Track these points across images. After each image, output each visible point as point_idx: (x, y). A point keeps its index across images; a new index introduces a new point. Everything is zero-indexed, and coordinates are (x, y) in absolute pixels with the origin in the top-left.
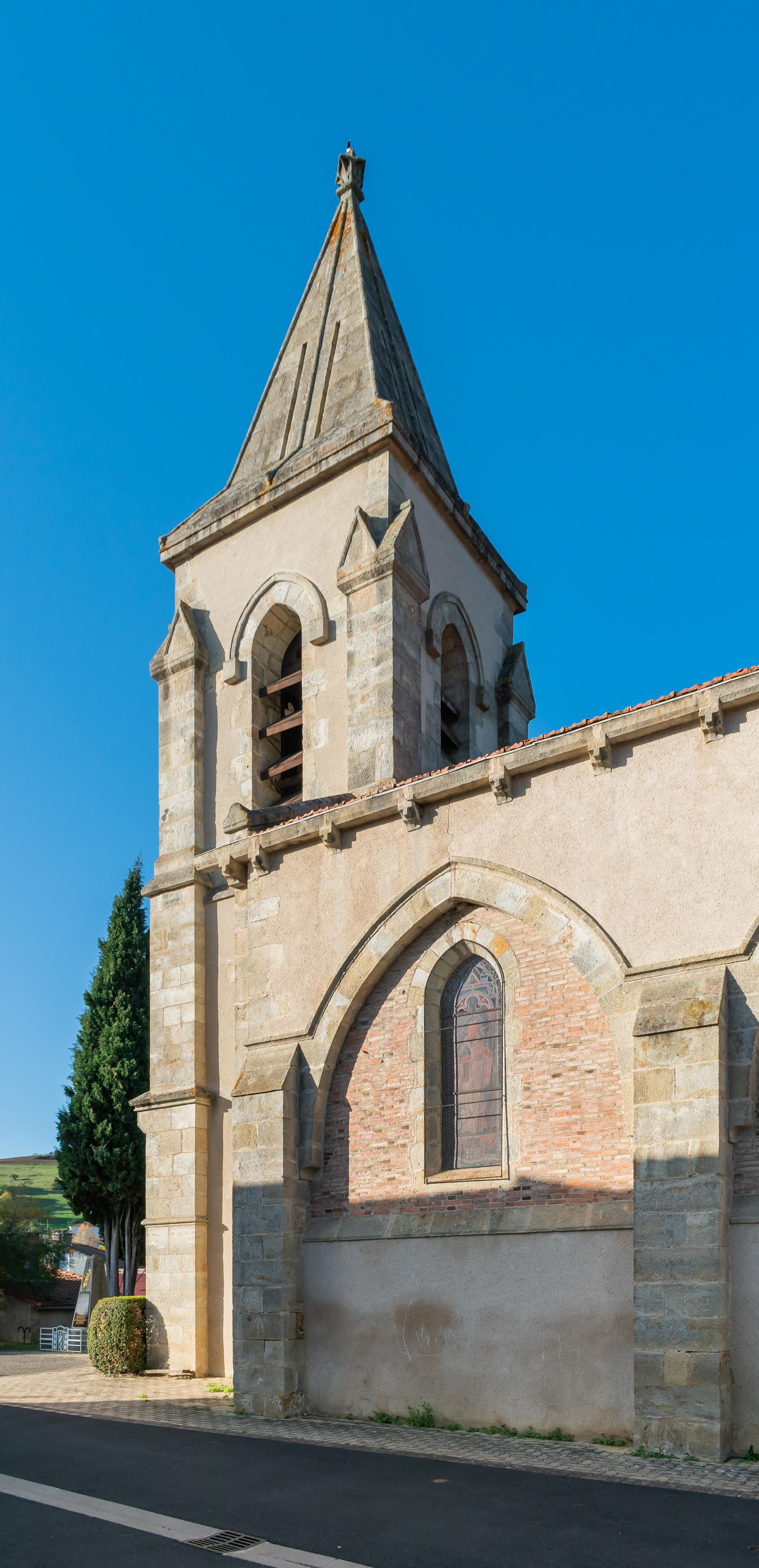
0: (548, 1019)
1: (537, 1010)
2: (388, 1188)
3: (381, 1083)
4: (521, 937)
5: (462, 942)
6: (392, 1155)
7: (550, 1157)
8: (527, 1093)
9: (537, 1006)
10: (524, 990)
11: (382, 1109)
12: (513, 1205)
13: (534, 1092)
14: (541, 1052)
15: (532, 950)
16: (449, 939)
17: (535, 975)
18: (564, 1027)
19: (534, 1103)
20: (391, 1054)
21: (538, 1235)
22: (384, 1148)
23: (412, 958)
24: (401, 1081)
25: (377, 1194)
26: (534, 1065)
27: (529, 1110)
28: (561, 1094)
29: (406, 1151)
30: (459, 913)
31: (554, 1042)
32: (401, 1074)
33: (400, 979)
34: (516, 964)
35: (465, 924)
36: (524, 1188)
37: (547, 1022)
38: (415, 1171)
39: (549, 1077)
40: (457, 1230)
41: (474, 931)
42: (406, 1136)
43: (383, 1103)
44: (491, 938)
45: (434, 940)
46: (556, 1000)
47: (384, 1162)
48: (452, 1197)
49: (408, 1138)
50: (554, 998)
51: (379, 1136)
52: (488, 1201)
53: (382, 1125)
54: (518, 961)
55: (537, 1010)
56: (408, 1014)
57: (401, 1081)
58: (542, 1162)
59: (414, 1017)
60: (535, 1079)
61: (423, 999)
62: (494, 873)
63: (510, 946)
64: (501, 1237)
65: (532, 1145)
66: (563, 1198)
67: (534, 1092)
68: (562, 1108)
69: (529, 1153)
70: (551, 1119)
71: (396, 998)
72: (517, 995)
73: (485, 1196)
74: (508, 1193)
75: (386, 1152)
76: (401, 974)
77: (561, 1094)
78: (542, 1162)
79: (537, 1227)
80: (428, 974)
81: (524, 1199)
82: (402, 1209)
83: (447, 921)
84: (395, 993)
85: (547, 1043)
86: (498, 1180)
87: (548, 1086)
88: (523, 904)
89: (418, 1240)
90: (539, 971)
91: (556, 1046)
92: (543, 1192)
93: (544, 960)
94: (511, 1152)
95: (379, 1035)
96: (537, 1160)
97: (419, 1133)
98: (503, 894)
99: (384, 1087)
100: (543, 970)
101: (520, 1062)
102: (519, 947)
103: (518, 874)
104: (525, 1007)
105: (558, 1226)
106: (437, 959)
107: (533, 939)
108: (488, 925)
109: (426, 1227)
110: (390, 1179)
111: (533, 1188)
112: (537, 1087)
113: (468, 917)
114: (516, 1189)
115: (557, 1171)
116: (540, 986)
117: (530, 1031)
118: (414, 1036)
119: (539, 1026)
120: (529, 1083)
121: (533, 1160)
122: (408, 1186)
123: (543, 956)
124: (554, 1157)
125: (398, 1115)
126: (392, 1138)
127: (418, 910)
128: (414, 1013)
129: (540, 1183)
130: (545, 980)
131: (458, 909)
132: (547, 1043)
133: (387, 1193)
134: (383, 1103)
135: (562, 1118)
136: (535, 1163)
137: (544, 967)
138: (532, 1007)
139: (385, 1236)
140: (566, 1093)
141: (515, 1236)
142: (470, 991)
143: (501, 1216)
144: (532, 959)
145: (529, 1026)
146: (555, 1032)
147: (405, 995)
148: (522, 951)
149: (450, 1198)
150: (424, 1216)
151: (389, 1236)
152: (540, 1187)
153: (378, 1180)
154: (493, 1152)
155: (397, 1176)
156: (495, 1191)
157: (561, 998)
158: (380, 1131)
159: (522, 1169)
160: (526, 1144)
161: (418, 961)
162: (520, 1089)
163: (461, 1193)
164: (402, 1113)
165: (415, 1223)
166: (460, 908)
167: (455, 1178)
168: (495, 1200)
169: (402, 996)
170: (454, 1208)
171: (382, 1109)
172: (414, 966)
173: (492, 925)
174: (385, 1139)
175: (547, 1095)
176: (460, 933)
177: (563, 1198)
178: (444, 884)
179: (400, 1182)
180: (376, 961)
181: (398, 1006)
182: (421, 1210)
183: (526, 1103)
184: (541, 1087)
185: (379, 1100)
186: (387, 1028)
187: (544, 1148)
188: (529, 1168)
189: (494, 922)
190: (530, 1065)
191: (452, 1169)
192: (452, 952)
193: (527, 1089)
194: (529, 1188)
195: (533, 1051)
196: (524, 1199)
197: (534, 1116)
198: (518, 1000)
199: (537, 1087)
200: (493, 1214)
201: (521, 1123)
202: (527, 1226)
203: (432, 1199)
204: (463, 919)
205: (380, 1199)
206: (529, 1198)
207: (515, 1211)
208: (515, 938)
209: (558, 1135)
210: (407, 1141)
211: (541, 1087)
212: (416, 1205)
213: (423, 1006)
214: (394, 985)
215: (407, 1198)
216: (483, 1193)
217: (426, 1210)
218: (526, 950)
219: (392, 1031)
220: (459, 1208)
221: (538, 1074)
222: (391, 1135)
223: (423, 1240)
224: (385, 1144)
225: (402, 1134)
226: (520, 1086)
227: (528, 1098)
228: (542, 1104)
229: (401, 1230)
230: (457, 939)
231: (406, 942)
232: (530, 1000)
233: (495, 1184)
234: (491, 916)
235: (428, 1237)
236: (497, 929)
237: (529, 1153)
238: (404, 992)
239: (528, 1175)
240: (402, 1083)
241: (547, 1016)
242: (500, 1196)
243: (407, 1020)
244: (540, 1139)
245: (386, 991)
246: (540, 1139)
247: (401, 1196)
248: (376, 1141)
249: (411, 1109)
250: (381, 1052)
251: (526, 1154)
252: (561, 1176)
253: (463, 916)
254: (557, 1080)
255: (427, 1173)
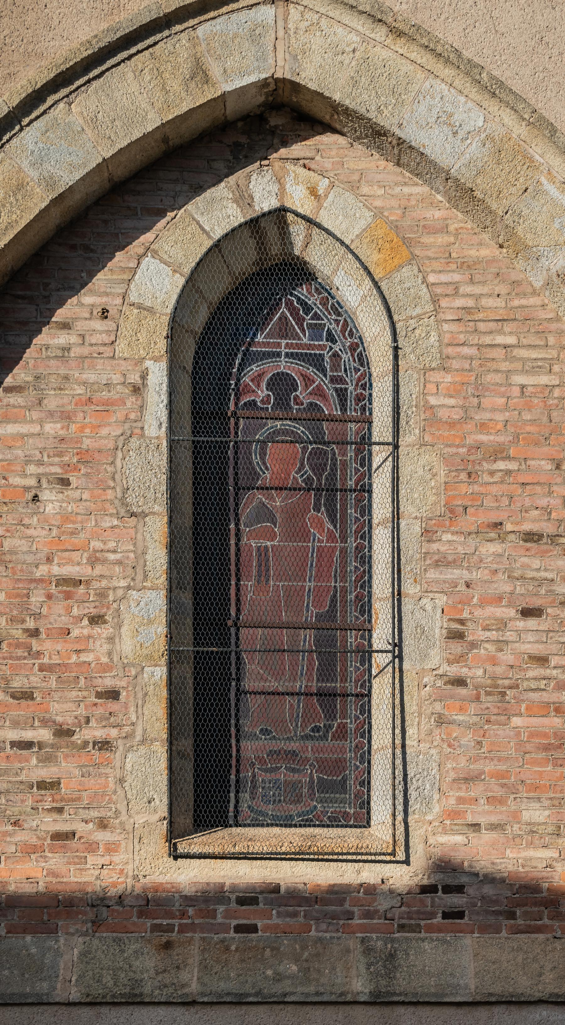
0: (512, 466)
1: (484, 438)
2: (55, 861)
3: (29, 558)
4: (442, 239)
5: (280, 215)
6: (66, 769)
7: (516, 816)
8: (457, 648)
9: (483, 427)
10: (448, 378)
11: (35, 633)
12: (416, 929)
13: (473, 645)
14: (494, 548)
15: (472, 281)
16: (243, 198)
17: (479, 347)
18: (550, 493)
19: (476, 673)
20: (65, 482)
21: (497, 1010)
22: (41, 745)
23: (129, 223)
24: (93, 561)
25: (17, 876)
26: (475, 575)
27: (462, 691)
28: (542, 660)
29: (109, 763)
30: (273, 132)
31: (527, 527)
32: (96, 544)
33: (92, 275)
34: (429, 307)
35: (290, 166)
36: (448, 889)
37: (508, 472)
38: (140, 819)
39: (512, 613)
40: (278, 989)
41: (313, 192)
42: (108, 719)
43: (37, 616)
44: (363, 224)
45: (198, 189)
46: (533, 422)
47: (42, 785)
48: (248, 898)
49: (117, 726)
50: (527, 416)
51: (22, 710)
52: (350, 916)
53: (35, 680)
54: (435, 300)
55: (484, 438)
56: (117, 378)
57: (93, 561)
58: (493, 827)
59: (137, 390)
60: (478, 613)
61: (162, 345)
62: (401, 46)
63: (414, 257)
64: (401, 1010)
65: (469, 779)
66: (546, 921)
67: (473, 645)
68: (545, 697)
69: (461, 800)
70: (516, 721)
71: (80, 326)
72: (431, 388)
73: (341, 902)
74: (403, 898)
75: (48, 759)
76: (96, 261)
77: (542, 660)
78: (493, 827)
79: (497, 989)
80: (181, 281)
81: (445, 916)
82: (97, 924)
83: (237, 145)
84: (76, 308)
85: (509, 527)
86: (370, 860)
87: (510, 635)
88: (474, 148)
89: (162, 1011)
90: (487, 340)
91: (531, 537)
92: (496, 902)
93: (501, 314)
94: (413, 794)
95: (24, 421)
96: (482, 820)
97: (152, 716)
98: (422, 108)
99: (42, 571)
100: (500, 340)
101: (437, 564)
102: (436, 265)
103: (471, 70)
104: (452, 425)
105: (550, 989)
106: (208, 244)
107: (473, 253)
108: (353, 187)
109: (184, 976)
110: (57, 836)
111: (471, 891)
112: (483, 635)
113: (298, 149)
114: (426, 890)
115: (531, 853)
116: (490, 378)
117: (464, 488)
118: (134, 443)
119: (486, 478)
120: (462, 622)
121: (470, 819)
122: (117, 858)
123: (500, 303)
124: (526, 816)
125: (84, 657)
126: (68, 720)
127: (175, 85)
128: (134, 378)
129: (489, 879)
130: (504, 366)
131: (279, 116)
132: (509, 527)
133: (52, 873)
134: (37, 616)
135: (546, 721)
136: (476, 827)
137: (500, 332)
138: (469, 427)
139: (59, 995)
140: (554, 661)
141: (437, 1010)
142: (270, 357)
143: (392, 956)
144: (470, 303)
145: (463, 476)
146: (528, 502)
147: (109, 325)
148: (444, 278)
149: (242, 901)
150: (168, 945)
151: (75, 995)
152: (488, 890)
153: (21, 837)
154: (337, 795)
155: (80, 828)
156: (370, 890)
157: (545, 419)
158: (27, 695)
159: (443, 839)
160: (452, 775)
161: (149, 236)
162: (438, 633)
163: (276, 889)
164: (98, 652)
165: (144, 964)
166: (275, 120)
167: (256, 848)
168: (368, 915)
169: (98, 325)
170: (253, 929)
171: (35, 633)
172: (136, 247)
173: (365, 190)
174: (45, 723)
175: (507, 657)
176: (275, 188)
177: (546, 921)
178: (255, 36)
179: (92, 847)
180: (40, 200)
181: (86, 351)
182: (156, 928)
183: (454, 670)
184: (493, 635)
185: (25, 607)
186: (51, 403)
187: (499, 792)
188: (459, 839)
189: (370, 183)
190: (466, 575)
191: (226, 825)
192: (246, 233)
193: (456, 636)
194: (460, 889)
195: (472, 542)
196: (445, 916)
197: (473, 708)
198: (433, 401)
199: (483, 635)
200: (368, 951)
201: (441, 721)
202: (469, 983)
203: (189, 900)
204: (283, 152)
205: (28, 889)
206: (460, 915)
207: (426, 946)
208: (427, 239)
209: (535, 762)
210: (114, 732)
211: (493, 635)
212: (141, 914)
213: (164, 365)
214: (75, 285)
215: (112, 892)
216: (337, 894)
217: (170, 929)
218: (456, 277)
219: (66, 417)
220: (266, 928)
221: (484, 602)
222: (63, 710)
223: (178, 1012)
224: (44, 734)
225: (100, 711)
226: (438, 626)
227: (459, 659)
228: (494, 678)
229: (108, 980)
230: (265, 202)
231: (120, 173)
232: (465, 409)
233: (369, 874)
234: (362, 165)
235: (193, 1003)
236: (378, 203)
237: (461, 800)
238: (105, 314)
239: (459, 856)
240: (99, 570)
241: (508, 458)
242: (383, 905)
243: (113, 395)
244: (489, 767)
245: (47, 299)
246: (489, 767)
247: (97, 886)
248: (16, 724)
249: (127, 646)
250: (32, 469)
251: (452, 801)
252: (541, 865)
253: (285, 143)
254: (532, 623)
255: (174, 833)
